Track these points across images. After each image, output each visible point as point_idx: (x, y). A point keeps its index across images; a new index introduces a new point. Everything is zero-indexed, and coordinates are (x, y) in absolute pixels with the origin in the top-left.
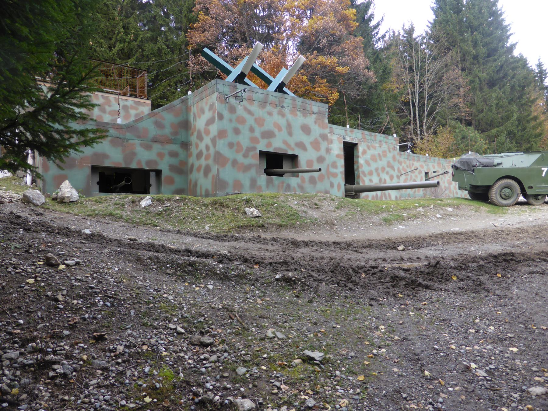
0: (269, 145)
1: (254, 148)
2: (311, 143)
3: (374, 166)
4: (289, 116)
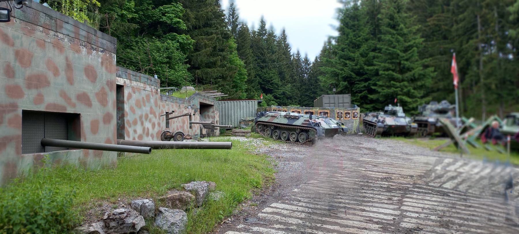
0: (39, 99)
1: (14, 107)
2: (97, 94)
3: (139, 112)
4: (71, 54)
